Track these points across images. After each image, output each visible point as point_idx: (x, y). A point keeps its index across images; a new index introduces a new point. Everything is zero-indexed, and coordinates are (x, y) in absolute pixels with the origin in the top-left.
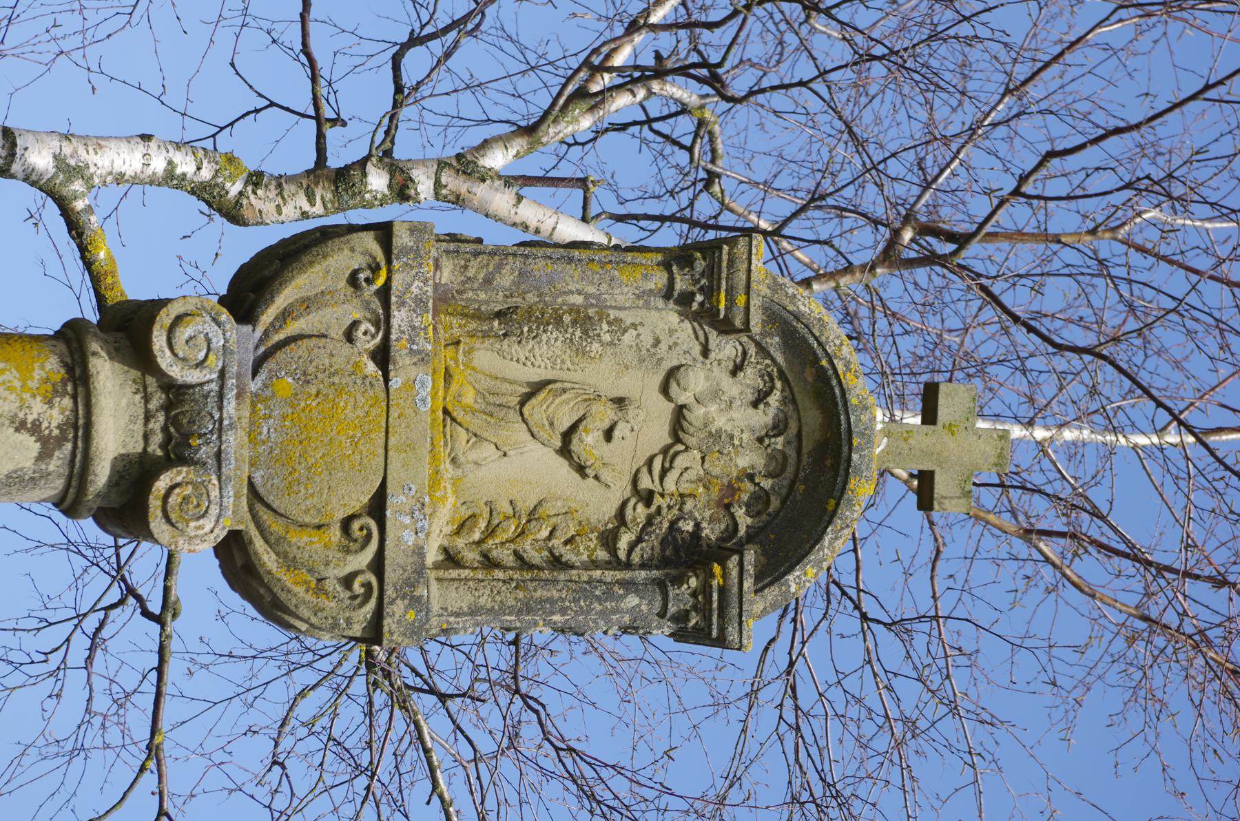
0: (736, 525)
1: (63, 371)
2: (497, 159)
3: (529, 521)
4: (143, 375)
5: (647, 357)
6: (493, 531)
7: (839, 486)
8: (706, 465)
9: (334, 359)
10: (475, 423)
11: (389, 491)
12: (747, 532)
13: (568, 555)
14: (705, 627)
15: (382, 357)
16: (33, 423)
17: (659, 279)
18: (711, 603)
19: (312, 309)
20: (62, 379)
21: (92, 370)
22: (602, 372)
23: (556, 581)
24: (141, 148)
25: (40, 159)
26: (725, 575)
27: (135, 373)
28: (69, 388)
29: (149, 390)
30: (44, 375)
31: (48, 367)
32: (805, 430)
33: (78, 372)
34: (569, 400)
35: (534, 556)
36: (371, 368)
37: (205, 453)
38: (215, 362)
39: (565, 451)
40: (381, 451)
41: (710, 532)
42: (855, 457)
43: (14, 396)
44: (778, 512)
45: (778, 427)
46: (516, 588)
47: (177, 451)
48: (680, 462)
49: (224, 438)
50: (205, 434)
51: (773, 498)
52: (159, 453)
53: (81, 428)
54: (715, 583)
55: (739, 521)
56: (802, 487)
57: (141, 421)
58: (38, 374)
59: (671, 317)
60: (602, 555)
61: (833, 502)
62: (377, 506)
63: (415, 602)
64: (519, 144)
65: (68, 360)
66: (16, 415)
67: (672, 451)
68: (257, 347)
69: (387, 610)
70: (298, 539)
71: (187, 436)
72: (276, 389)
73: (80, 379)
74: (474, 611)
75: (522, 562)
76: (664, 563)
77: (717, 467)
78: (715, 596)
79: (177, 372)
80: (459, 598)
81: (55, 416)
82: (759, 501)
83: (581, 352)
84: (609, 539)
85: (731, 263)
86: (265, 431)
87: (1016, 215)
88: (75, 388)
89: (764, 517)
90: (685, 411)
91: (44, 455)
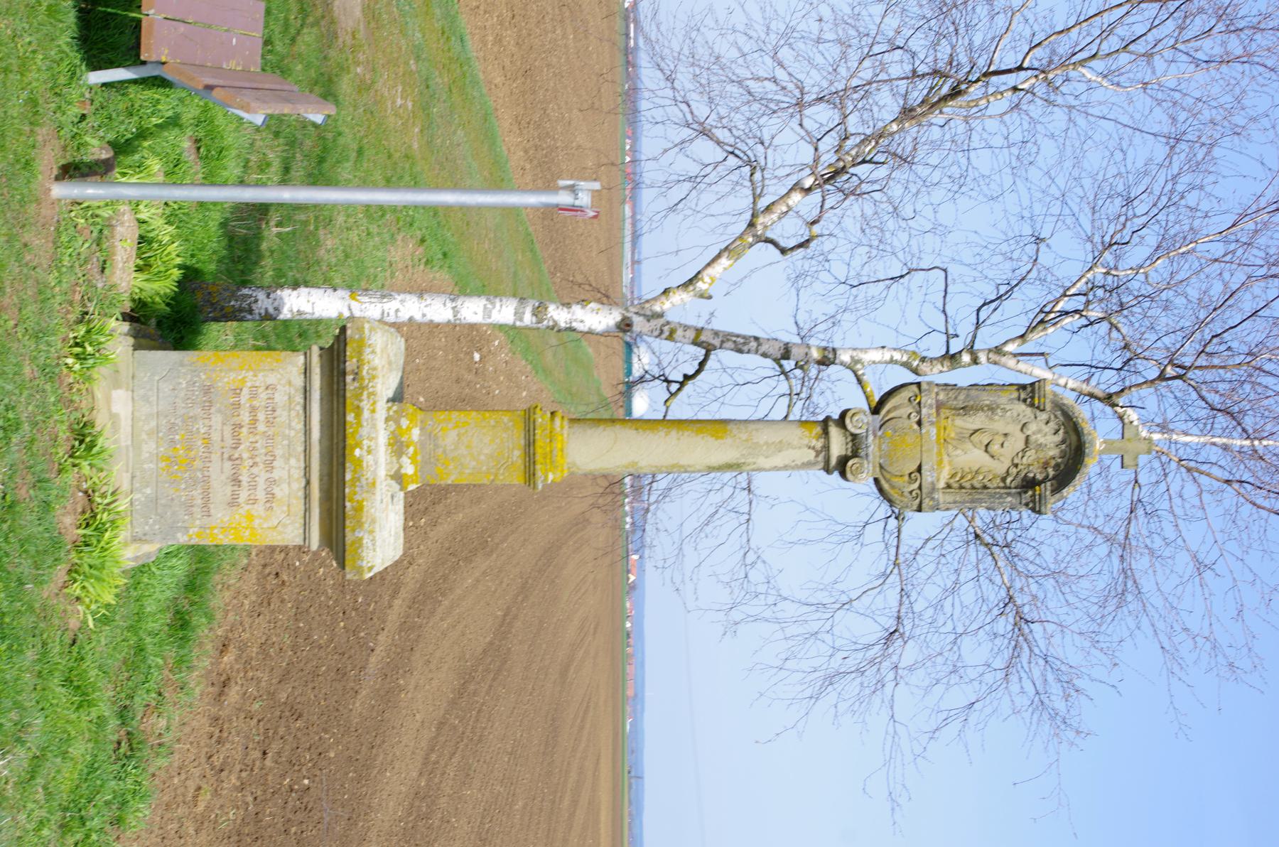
2: (1011, 348)
5: (1015, 420)
10: (954, 443)
13: (989, 485)
14: (1036, 507)
15: (919, 423)
17: (1015, 395)
22: (1000, 425)
24: (881, 351)
25: (845, 357)
35: (977, 485)
36: (916, 427)
37: (863, 454)
38: (865, 427)
39: (986, 451)
41: (1039, 477)
45: (1063, 442)
47: (855, 454)
48: (1028, 454)
53: (827, 448)
59: (1023, 406)
60: (1002, 485)
62: (919, 469)
63: (933, 499)
64: (1019, 341)
70: (895, 480)
74: (955, 502)
75: (973, 488)
76: (1023, 487)
77: (1041, 455)
79: (853, 430)
80: (950, 498)
81: (819, 444)
83: (991, 419)
84: (1004, 479)
87: (1202, 361)
91: (817, 456)
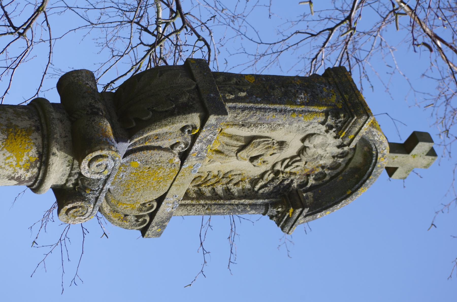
0: (307, 182)
1: (37, 156)
3: (223, 178)
4: (74, 159)
6: (206, 182)
7: (356, 187)
8: (306, 166)
9: (161, 158)
11: (167, 197)
12: (311, 186)
16: (18, 178)
18: (283, 218)
19: (159, 140)
20: (36, 160)
21: (51, 162)
23: (224, 205)
26: (293, 213)
27: (70, 158)
28: (38, 165)
29: (74, 166)
30: (28, 158)
31: (31, 154)
32: (353, 160)
33: (44, 159)
34: (260, 149)
37: (91, 197)
40: (169, 185)
42: (368, 181)
43: (11, 169)
44: (327, 182)
45: (343, 155)
46: (207, 209)
49: (101, 194)
50: (94, 191)
51: (327, 176)
52: (71, 186)
54: (288, 214)
55: (309, 181)
56: (341, 178)
57: (67, 175)
58: (25, 158)
61: (350, 191)
65: (41, 150)
66: (11, 175)
67: (294, 160)
68: (129, 147)
69: (150, 228)
71: (85, 188)
72: (131, 164)
73: (44, 162)
78: (286, 217)
82: (320, 177)
85: (355, 123)
86: (121, 175)
88: (41, 165)
89: (321, 182)
90: (307, 149)
